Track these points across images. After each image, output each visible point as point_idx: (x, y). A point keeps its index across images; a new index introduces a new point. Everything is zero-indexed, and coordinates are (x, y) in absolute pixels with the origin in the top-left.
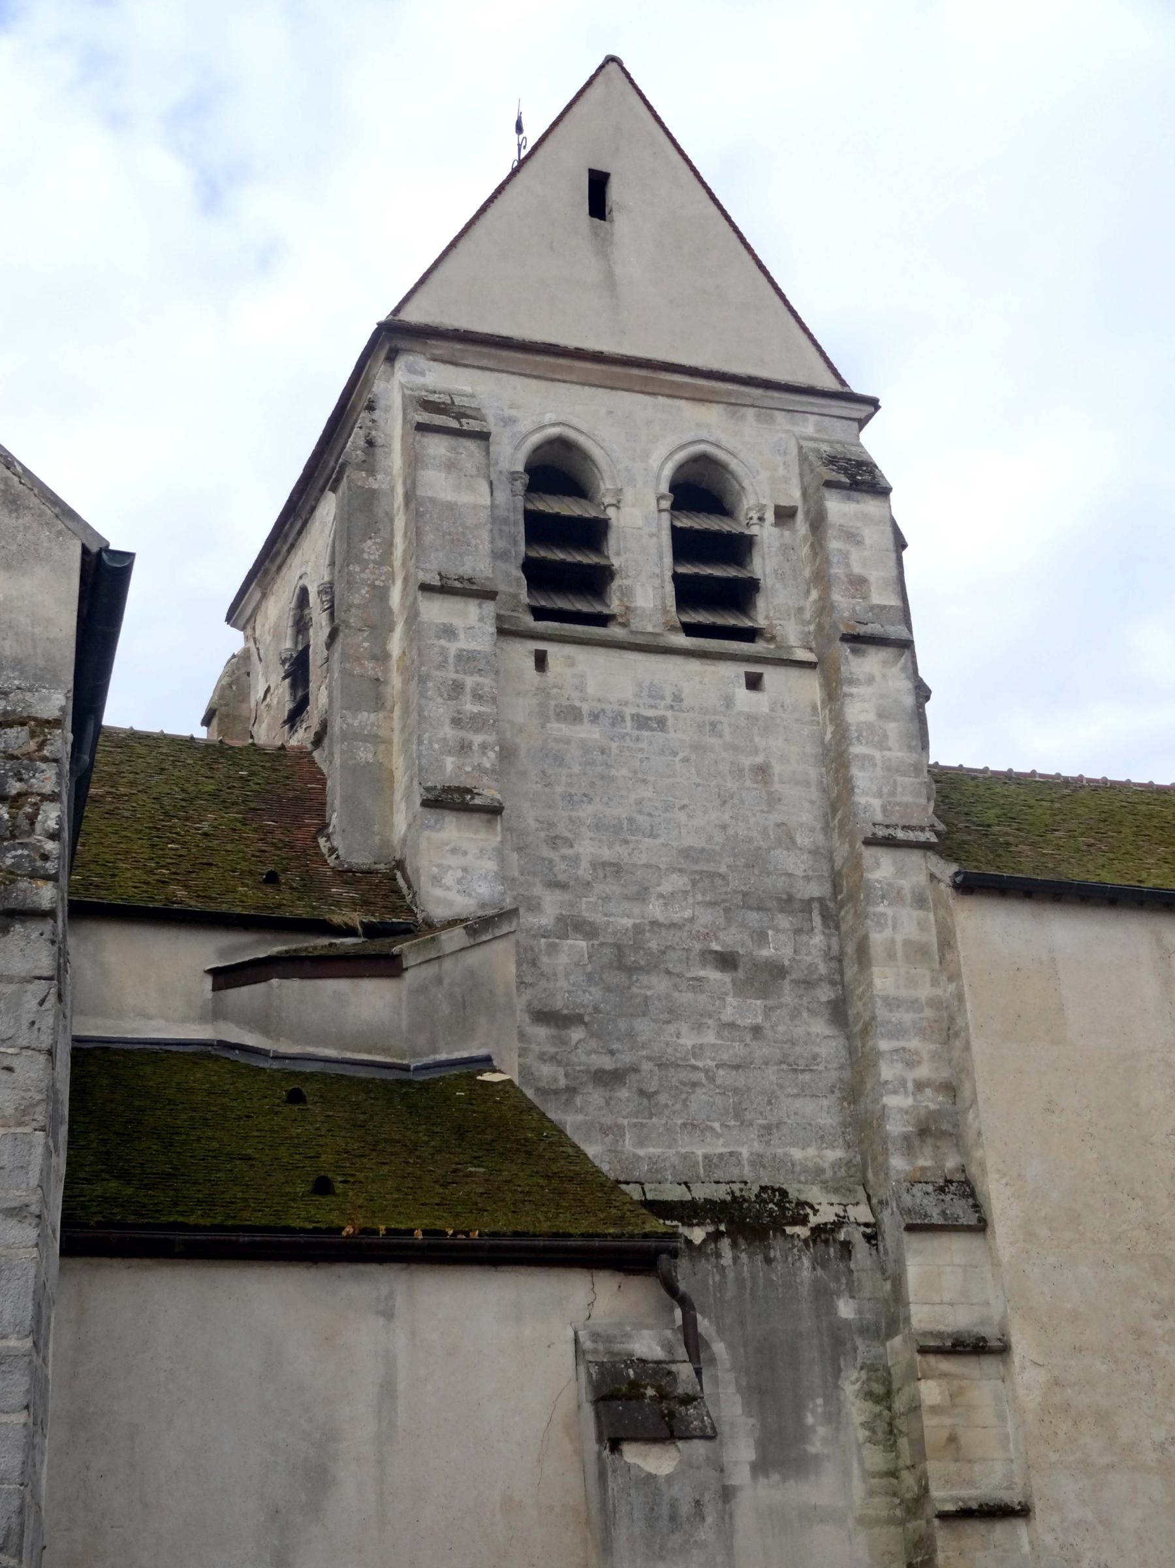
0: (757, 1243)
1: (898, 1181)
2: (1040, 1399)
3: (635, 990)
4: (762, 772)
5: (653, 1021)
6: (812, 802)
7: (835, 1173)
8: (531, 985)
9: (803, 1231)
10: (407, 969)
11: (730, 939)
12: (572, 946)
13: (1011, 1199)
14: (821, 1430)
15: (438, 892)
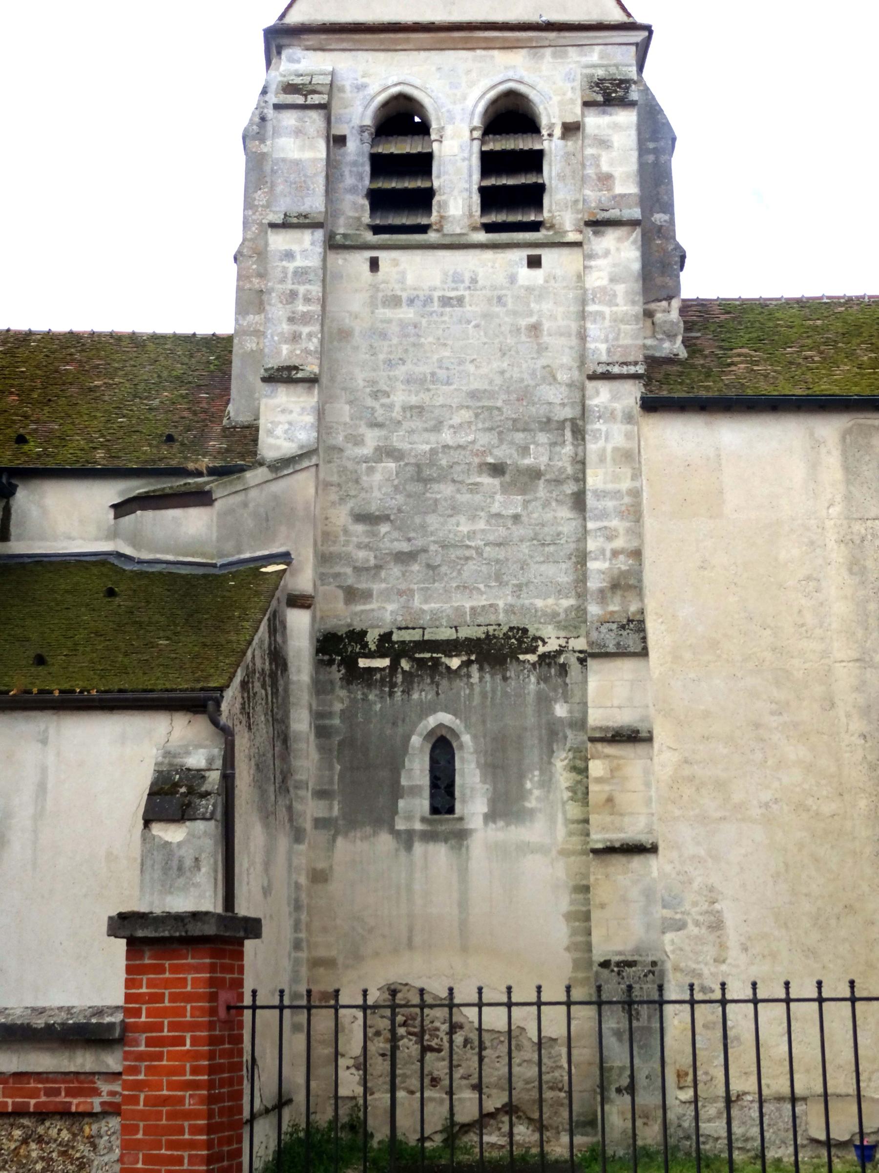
0: (498, 667)
1: (592, 622)
2: (671, 773)
3: (428, 495)
4: (535, 329)
5: (440, 515)
6: (571, 348)
7: (567, 615)
8: (355, 496)
9: (532, 658)
10: (216, 500)
11: (502, 453)
12: (385, 467)
13: (665, 633)
14: (537, 792)
15: (271, 441)
